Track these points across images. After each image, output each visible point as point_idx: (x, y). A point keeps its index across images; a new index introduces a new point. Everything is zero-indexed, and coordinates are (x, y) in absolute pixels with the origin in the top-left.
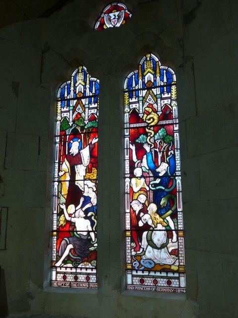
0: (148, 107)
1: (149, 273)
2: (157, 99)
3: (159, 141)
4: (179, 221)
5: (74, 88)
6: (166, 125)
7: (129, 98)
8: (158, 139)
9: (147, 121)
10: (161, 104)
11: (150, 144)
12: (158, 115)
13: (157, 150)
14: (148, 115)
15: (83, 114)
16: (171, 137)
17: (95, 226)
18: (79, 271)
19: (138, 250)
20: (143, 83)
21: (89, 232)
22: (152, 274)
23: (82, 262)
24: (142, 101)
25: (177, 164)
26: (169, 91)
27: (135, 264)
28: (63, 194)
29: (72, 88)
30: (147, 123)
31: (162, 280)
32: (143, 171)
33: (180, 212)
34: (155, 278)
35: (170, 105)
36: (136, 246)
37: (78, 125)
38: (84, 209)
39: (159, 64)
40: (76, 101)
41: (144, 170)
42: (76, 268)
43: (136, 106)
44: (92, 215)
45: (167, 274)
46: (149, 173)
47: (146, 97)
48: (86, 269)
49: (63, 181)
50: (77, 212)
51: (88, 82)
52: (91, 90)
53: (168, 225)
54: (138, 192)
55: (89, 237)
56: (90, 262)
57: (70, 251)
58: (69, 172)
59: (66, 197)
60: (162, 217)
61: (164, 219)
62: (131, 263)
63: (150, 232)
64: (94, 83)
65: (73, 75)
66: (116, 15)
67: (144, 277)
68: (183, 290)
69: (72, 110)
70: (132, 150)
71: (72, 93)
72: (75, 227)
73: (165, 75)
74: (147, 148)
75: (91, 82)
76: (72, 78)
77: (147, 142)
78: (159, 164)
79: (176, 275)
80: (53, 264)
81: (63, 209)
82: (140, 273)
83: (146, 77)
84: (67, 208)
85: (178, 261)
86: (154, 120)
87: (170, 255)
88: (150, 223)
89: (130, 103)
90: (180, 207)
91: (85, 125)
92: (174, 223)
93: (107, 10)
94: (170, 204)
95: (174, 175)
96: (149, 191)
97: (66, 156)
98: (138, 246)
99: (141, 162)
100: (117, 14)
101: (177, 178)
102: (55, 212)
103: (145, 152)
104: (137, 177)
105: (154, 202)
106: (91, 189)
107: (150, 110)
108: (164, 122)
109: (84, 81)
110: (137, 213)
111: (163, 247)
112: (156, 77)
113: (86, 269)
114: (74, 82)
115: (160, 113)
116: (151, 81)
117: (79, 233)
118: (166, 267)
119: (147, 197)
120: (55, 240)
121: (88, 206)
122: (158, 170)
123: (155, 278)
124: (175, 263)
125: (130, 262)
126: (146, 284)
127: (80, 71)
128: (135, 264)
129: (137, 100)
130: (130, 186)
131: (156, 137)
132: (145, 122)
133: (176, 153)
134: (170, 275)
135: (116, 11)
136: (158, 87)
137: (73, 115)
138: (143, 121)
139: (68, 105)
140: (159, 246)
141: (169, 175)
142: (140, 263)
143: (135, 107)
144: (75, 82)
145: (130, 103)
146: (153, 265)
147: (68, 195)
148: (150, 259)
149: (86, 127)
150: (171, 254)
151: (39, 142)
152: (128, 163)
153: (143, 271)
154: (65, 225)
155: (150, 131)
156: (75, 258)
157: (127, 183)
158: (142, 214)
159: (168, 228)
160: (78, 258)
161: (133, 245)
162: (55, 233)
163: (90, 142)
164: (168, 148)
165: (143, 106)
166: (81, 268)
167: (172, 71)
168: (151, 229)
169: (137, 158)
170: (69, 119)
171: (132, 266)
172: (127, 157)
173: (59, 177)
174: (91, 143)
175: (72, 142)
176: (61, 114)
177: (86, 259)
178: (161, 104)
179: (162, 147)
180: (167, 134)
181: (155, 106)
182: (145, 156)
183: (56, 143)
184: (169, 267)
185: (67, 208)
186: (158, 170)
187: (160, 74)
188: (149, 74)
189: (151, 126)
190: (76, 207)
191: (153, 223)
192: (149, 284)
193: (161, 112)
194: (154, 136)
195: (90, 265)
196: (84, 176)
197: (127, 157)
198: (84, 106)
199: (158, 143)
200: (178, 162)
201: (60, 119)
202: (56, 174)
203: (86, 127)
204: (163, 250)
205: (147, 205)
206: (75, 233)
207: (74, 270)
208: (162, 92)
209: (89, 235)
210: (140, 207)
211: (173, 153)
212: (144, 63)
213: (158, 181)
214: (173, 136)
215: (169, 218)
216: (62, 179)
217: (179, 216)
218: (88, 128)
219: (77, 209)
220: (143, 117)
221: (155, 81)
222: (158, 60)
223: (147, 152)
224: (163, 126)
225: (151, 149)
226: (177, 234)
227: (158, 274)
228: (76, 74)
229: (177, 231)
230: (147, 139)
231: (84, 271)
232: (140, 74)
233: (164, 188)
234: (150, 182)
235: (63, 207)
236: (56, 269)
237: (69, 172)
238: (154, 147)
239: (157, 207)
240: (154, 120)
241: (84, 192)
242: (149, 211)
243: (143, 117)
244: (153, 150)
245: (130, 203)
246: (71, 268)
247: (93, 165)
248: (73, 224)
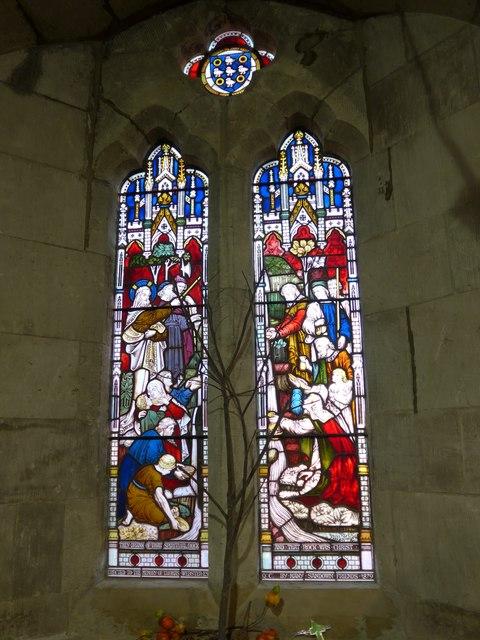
10: (320, 231)
43: (277, 227)
120: (114, 484)
129: (278, 218)
143: (275, 229)
178: (325, 228)
188: (301, 170)
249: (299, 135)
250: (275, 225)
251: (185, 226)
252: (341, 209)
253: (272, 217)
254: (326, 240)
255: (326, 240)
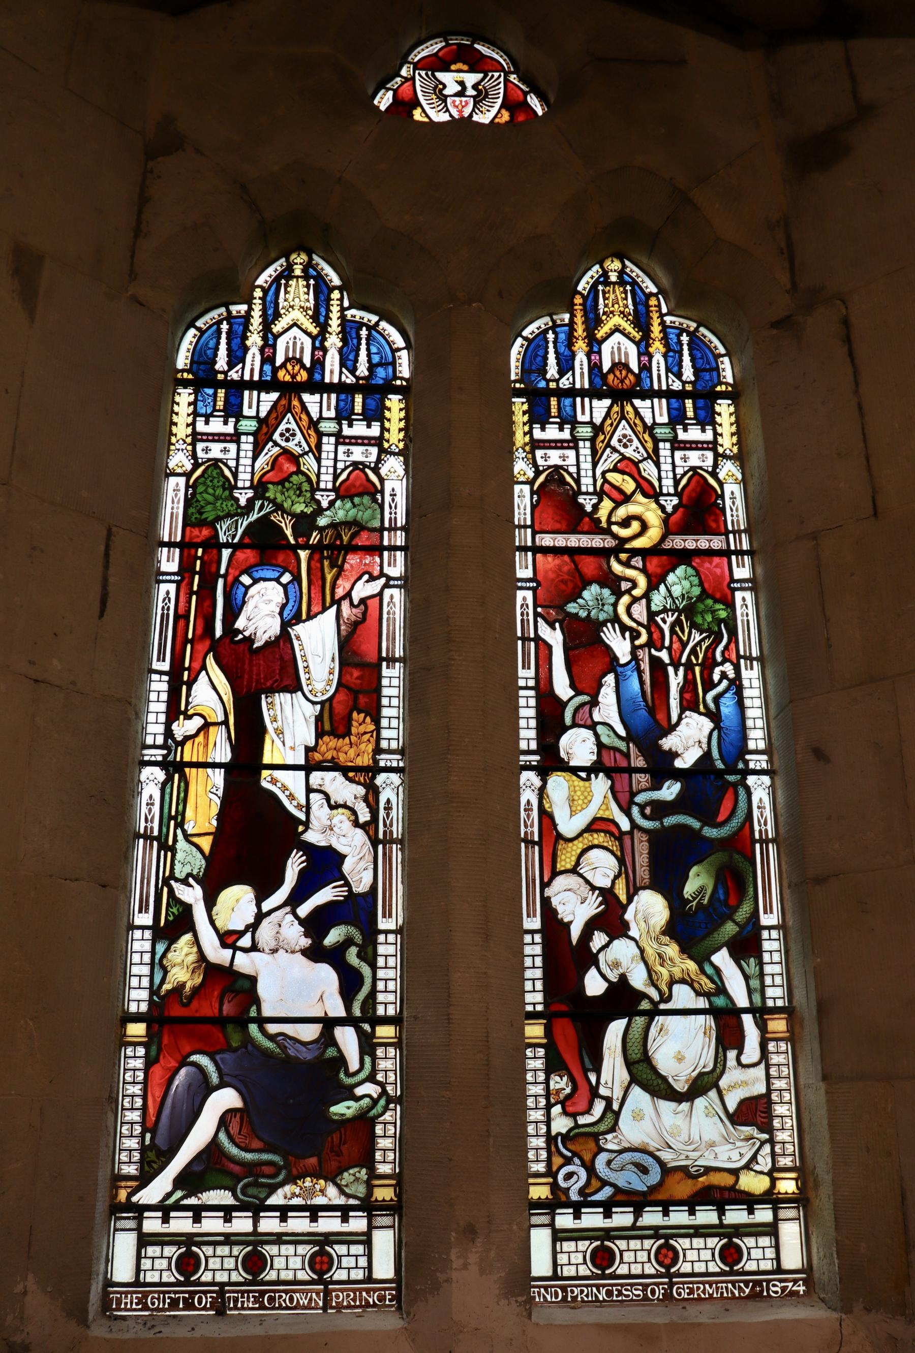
0: (615, 469)
1: (638, 1214)
2: (656, 441)
3: (670, 619)
4: (768, 969)
5: (265, 338)
6: (698, 552)
7: (531, 422)
8: (665, 610)
9: (615, 528)
11: (631, 629)
12: (663, 508)
13: (664, 655)
14: (618, 504)
15: (309, 463)
16: (719, 606)
17: (361, 996)
18: (269, 1224)
19: (582, 1106)
20: (595, 368)
21: (329, 1024)
22: (652, 1217)
23: (292, 1179)
24: (593, 440)
25: (750, 723)
26: (707, 419)
27: (569, 1176)
28: (190, 828)
29: (254, 340)
30: (615, 536)
31: (698, 1242)
32: (600, 745)
33: (770, 928)
34: (668, 1237)
35: (714, 474)
36: (575, 1089)
37: (279, 507)
38: (304, 910)
39: (659, 306)
40: (274, 396)
41: (605, 740)
42: (257, 1209)
43: (564, 458)
44: (348, 942)
45: (721, 1213)
46: (627, 756)
47: (608, 428)
48: (314, 1212)
49: (192, 765)
50: (265, 922)
51: (335, 324)
52: (348, 361)
53: (722, 990)
54: (580, 835)
55: (331, 1052)
56: (332, 1177)
57: (224, 1121)
58: (226, 722)
59: (206, 843)
60: (694, 951)
61: (702, 959)
62: (551, 1173)
63: (639, 1021)
64: (364, 332)
65: (260, 281)
66: (469, 85)
67: (612, 1239)
68: (795, 1281)
69: (254, 434)
70: (549, 647)
71: (253, 358)
72: (256, 1001)
73: (686, 352)
74: (621, 647)
75: (349, 330)
76: (258, 293)
77: (616, 619)
78: (674, 718)
79: (764, 1215)
80: (123, 1195)
81: (187, 909)
82: (592, 1219)
83: (606, 348)
84: (210, 902)
85: (767, 1149)
86: (645, 527)
87: (733, 1123)
88: (638, 979)
89: (536, 444)
90: (768, 910)
91: (320, 511)
92: (747, 978)
93: (423, 54)
94: (727, 894)
95: (741, 766)
96: (630, 833)
97: (216, 648)
98: (584, 1091)
99: (594, 703)
100: (471, 79)
101: (751, 780)
102: (146, 919)
103: (612, 663)
104: (575, 771)
105: (654, 886)
106: (341, 816)
107: (629, 485)
108: (690, 543)
109: (315, 318)
110: (575, 932)
111: (702, 1092)
112: (651, 357)
113: (314, 1212)
114: (264, 310)
115: (670, 503)
116: (626, 366)
117: (272, 1028)
118: (717, 1179)
119: (621, 861)
121: (325, 895)
122: (668, 743)
123: (668, 1237)
124: (754, 1158)
125: (541, 1167)
126: (623, 1270)
127: (298, 271)
128: (569, 1176)
130: (543, 812)
131: (658, 599)
132: (608, 532)
133: (745, 674)
134: (736, 1216)
135: (465, 68)
136: (660, 394)
137: (255, 458)
138: (596, 528)
139: (233, 411)
140: (681, 1086)
141: (720, 765)
142: (591, 1170)
143: (220, 456)
144: (271, 316)
145: (536, 444)
146: (655, 1176)
147: (219, 836)
148: (643, 1151)
149: (322, 522)
150: (738, 1117)
151: (107, 555)
152: (533, 702)
153: (608, 1209)
154: (196, 990)
155: (630, 573)
156: (249, 1156)
157: (528, 796)
158: (599, 939)
159: (720, 1001)
160: (265, 1157)
161: (560, 1083)
162: (137, 1030)
163: (340, 592)
164: (712, 649)
165: (595, 465)
166: (284, 1212)
167: (716, 342)
168: (645, 1005)
169: (573, 686)
170: (235, 475)
171: (554, 1186)
172: (526, 675)
173: (170, 740)
174: (348, 595)
175: (246, 580)
176: (193, 444)
177: (313, 1161)
179: (684, 645)
180: (704, 591)
181: (649, 469)
182: (610, 679)
183: (159, 576)
184: (729, 1180)
185: (210, 902)
186: (668, 743)
187: (667, 345)
188: (617, 337)
189: (635, 552)
190: (260, 898)
191: (652, 981)
192: (636, 1269)
193: (675, 501)
194: (647, 596)
195: (332, 1191)
196: (308, 750)
197: (526, 675)
198: (314, 424)
199: (666, 628)
200: (755, 713)
201: (188, 466)
202: (154, 730)
203: (322, 522)
204: (700, 1102)
205: (623, 898)
206: (253, 1028)
207: (242, 1224)
208: (677, 419)
209: (327, 1038)
210: (591, 907)
211: (731, 674)
212: (594, 287)
213: (670, 791)
214: (730, 605)
215: (722, 959)
216: (189, 753)
217: (766, 946)
218: (333, 525)
219: (266, 906)
220: (596, 507)
221: (646, 368)
222: (519, 341)
223: (616, 659)
224: (684, 557)
225: (634, 649)
226: (762, 1027)
227: (679, 1217)
228: (277, 280)
229: (761, 1013)
230: (615, 605)
231: (299, 1224)
232: (580, 330)
233: (696, 824)
234: (633, 795)
235: (192, 895)
236: (140, 1220)
237: (226, 722)
238: (650, 644)
239: (671, 908)
240: (645, 527)
241: (307, 824)
242: (633, 925)
243: (596, 507)
244: (643, 655)
245: (544, 885)
246: (227, 1212)
247: (355, 700)
248: (246, 984)
249: (299, 259)
250: (222, 445)
251: (677, 445)
252: (232, 420)
253: (552, 433)
254: (676, 494)
255: (334, 489)
